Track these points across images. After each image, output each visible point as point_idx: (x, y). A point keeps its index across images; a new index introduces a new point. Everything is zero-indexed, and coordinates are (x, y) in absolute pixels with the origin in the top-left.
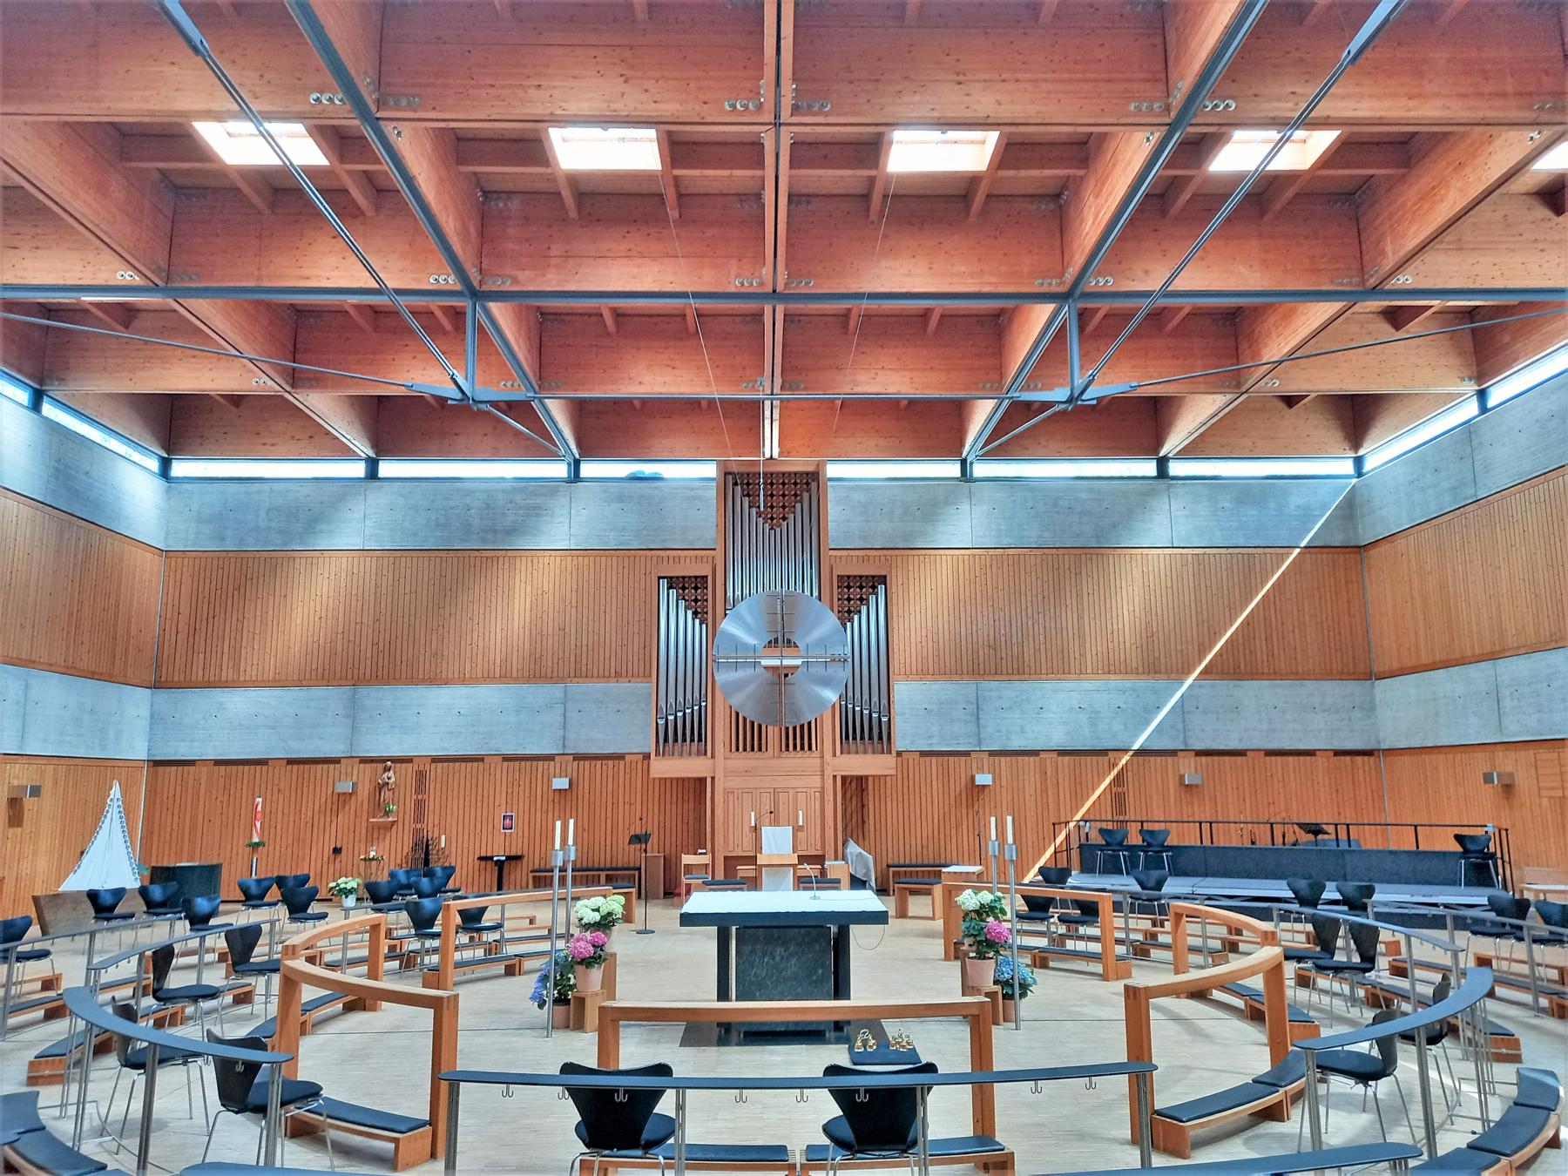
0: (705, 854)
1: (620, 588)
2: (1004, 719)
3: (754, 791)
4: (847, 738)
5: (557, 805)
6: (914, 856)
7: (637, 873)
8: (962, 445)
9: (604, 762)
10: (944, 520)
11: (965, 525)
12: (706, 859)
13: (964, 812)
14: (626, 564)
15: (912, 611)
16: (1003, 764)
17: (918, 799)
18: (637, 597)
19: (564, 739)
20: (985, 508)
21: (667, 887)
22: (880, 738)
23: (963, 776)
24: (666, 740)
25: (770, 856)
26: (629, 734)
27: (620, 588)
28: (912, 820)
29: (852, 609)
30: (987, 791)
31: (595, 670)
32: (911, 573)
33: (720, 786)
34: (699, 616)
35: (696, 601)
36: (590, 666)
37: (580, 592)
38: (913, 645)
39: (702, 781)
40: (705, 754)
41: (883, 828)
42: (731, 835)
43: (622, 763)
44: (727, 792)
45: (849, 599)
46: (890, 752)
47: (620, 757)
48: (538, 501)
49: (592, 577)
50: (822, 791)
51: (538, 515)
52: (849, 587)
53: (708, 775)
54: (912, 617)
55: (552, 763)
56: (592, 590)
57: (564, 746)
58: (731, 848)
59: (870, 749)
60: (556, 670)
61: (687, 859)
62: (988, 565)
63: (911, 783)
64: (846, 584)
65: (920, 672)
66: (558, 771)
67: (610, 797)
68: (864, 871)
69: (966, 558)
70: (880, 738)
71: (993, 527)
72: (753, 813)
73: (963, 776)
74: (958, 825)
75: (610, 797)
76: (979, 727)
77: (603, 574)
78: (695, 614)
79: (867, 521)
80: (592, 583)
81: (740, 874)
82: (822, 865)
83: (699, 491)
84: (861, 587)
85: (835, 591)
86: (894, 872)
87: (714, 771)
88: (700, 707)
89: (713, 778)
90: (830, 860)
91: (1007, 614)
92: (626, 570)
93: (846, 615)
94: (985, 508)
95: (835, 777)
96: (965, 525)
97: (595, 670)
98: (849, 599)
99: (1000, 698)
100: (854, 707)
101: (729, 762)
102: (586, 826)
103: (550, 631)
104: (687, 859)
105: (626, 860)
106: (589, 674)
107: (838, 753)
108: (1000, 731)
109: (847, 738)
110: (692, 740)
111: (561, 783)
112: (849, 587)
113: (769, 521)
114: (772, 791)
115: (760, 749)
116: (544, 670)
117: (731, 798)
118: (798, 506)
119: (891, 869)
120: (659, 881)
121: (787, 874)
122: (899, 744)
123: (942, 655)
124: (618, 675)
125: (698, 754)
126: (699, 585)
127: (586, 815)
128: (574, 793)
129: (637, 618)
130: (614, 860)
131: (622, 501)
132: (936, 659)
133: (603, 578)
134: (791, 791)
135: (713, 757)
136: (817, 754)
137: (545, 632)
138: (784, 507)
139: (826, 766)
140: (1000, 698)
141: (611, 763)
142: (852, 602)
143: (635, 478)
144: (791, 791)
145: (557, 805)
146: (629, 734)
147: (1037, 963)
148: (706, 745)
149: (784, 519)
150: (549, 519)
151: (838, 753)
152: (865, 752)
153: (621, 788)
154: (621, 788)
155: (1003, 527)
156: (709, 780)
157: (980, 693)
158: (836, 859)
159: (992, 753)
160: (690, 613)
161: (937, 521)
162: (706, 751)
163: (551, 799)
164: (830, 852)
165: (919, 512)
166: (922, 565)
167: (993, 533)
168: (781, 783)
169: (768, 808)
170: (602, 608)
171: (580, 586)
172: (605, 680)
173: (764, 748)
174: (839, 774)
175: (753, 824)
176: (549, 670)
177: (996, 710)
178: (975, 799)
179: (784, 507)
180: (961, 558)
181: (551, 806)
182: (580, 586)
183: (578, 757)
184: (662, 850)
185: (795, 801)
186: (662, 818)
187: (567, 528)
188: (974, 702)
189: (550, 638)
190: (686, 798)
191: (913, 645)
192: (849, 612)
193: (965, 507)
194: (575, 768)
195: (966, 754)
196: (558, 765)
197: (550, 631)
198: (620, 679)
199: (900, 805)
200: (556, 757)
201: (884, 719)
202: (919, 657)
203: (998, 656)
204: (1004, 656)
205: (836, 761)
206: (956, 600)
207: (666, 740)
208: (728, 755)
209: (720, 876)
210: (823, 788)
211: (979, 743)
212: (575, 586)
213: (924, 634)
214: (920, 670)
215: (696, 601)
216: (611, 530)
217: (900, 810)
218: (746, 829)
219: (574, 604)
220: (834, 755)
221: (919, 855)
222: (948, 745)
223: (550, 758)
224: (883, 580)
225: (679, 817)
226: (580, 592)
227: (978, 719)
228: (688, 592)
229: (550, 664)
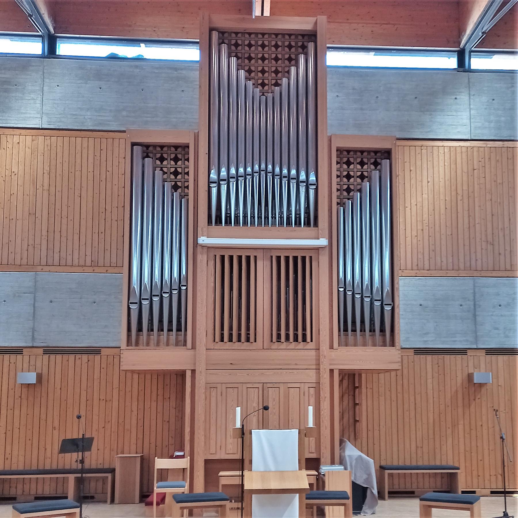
0: (183, 457)
1: (97, 172)
2: (502, 316)
3: (219, 386)
4: (346, 330)
5: (24, 402)
6: (408, 457)
7: (109, 476)
8: (461, 31)
9: (78, 356)
10: (442, 110)
11: (464, 117)
12: (183, 463)
13: (460, 410)
14: (104, 147)
15: (408, 204)
16: (500, 364)
17: (412, 399)
18: (115, 182)
19: (34, 330)
20: (484, 99)
21: (145, 489)
22: (382, 330)
23: (459, 374)
24: (140, 329)
25: (265, 474)
26: (106, 326)
27: (97, 172)
28: (407, 420)
29: (352, 187)
30: (483, 390)
31: (69, 258)
32: (407, 165)
33: (201, 380)
34: (179, 190)
35: (176, 173)
36: (63, 254)
37: (53, 175)
38: (409, 239)
39: (182, 374)
40: (185, 344)
41: (376, 427)
42: (213, 436)
43: (98, 357)
44: (211, 387)
45: (348, 177)
46: (393, 344)
47: (95, 351)
48: (7, 75)
49: (66, 158)
50: (318, 385)
51: (6, 91)
52: (348, 163)
53: (186, 366)
54: (408, 210)
55: (19, 357)
56: (66, 173)
57: (33, 339)
58: (213, 451)
59: (370, 342)
60: (25, 256)
61: (161, 463)
62: (487, 157)
63: (405, 381)
64: (345, 160)
65: (415, 267)
66: (26, 365)
67: (84, 393)
68: (365, 476)
69: (464, 150)
70: (382, 330)
71: (492, 118)
72: (238, 409)
73: (459, 374)
74: (455, 425)
75: (84, 393)
76: (475, 323)
77: (78, 156)
78: (175, 188)
79: (362, 109)
80: (66, 165)
81: (223, 481)
82: (317, 469)
83: (184, 72)
84: (362, 164)
85: (335, 166)
86: (389, 474)
87: (195, 364)
88: (180, 290)
89: (193, 371)
90: (326, 464)
91: (506, 208)
92: (104, 153)
93: (345, 193)
94: (484, 99)
95: (332, 371)
96: (464, 117)
97: (69, 258)
98: (348, 177)
99: (498, 294)
100: (372, 303)
101: (212, 353)
102: (56, 424)
103: (19, 216)
104: (161, 463)
105: (101, 461)
106: (63, 262)
107: (336, 345)
108: (497, 329)
109: (346, 330)
110: (170, 330)
111: (31, 378)
112: (348, 163)
113: (260, 87)
114: (260, 386)
115: (248, 340)
116: (11, 256)
117: (213, 394)
118: (293, 69)
119: (387, 472)
120: (134, 484)
121: (290, 503)
122: (224, 341)
123: (438, 249)
124: (94, 265)
125: (177, 344)
126: (180, 156)
127: (57, 413)
128: (44, 389)
129: (115, 204)
130: (41, 458)
131: (100, 79)
132: (432, 254)
133: (78, 161)
134: (282, 386)
135: (193, 347)
136: (312, 345)
137: (13, 216)
138: (276, 72)
139: (322, 359)
140: (498, 294)
141: (85, 357)
142: (352, 180)
143: (113, 57)
144: (282, 386)
145: (24, 402)
146: (106, 326)
147: (282, 424)
148: (185, 335)
149: (277, 84)
150: (19, 95)
151: (336, 345)
152: (365, 345)
153: (96, 383)
154: (96, 383)
155: (503, 119)
156: (188, 374)
157: (477, 290)
158: (333, 463)
159: (490, 352)
160: (168, 186)
161: (435, 111)
162: (185, 341)
163: (18, 394)
164: (326, 455)
165: (416, 102)
166: (419, 156)
167: (492, 125)
168: (272, 377)
169: (255, 405)
170: (77, 193)
171: (53, 168)
172: (80, 269)
173: (252, 339)
174: (337, 367)
175: (238, 425)
176: (18, 257)
177: (494, 307)
178: (472, 398)
179: (276, 72)
180: (458, 149)
181: (18, 401)
182: (53, 168)
183: (49, 351)
184: (140, 450)
185: (287, 396)
186: (141, 416)
187: (38, 105)
188: (472, 298)
189: (19, 223)
190: (167, 396)
191: (409, 239)
192: (348, 190)
193: (464, 98)
194: (46, 362)
195: (463, 352)
196: (26, 358)
197: (19, 216)
198: (97, 269)
199: (394, 404)
200: (24, 350)
201: (388, 308)
202: (415, 251)
203: (496, 252)
204: (502, 252)
205: (333, 354)
206: (454, 193)
207: (140, 329)
208: (211, 345)
209: (199, 488)
210: (318, 383)
211: (476, 339)
212: (47, 168)
213: (420, 227)
214: (415, 264)
215: (176, 173)
216: (88, 110)
217: (394, 409)
218: (230, 432)
219: (46, 187)
220: (331, 347)
221: (414, 455)
222: (443, 343)
223: (17, 351)
224: (387, 154)
225: (160, 416)
226: (53, 175)
227: (475, 316)
228: (169, 165)
229: (18, 250)
